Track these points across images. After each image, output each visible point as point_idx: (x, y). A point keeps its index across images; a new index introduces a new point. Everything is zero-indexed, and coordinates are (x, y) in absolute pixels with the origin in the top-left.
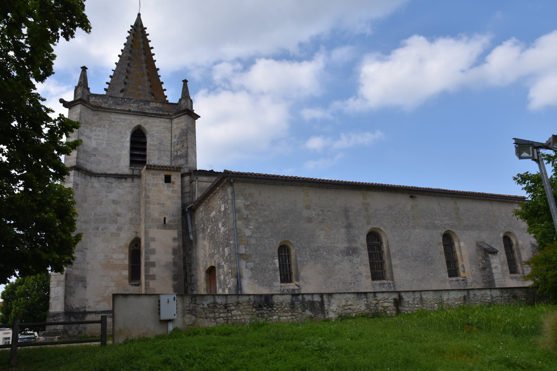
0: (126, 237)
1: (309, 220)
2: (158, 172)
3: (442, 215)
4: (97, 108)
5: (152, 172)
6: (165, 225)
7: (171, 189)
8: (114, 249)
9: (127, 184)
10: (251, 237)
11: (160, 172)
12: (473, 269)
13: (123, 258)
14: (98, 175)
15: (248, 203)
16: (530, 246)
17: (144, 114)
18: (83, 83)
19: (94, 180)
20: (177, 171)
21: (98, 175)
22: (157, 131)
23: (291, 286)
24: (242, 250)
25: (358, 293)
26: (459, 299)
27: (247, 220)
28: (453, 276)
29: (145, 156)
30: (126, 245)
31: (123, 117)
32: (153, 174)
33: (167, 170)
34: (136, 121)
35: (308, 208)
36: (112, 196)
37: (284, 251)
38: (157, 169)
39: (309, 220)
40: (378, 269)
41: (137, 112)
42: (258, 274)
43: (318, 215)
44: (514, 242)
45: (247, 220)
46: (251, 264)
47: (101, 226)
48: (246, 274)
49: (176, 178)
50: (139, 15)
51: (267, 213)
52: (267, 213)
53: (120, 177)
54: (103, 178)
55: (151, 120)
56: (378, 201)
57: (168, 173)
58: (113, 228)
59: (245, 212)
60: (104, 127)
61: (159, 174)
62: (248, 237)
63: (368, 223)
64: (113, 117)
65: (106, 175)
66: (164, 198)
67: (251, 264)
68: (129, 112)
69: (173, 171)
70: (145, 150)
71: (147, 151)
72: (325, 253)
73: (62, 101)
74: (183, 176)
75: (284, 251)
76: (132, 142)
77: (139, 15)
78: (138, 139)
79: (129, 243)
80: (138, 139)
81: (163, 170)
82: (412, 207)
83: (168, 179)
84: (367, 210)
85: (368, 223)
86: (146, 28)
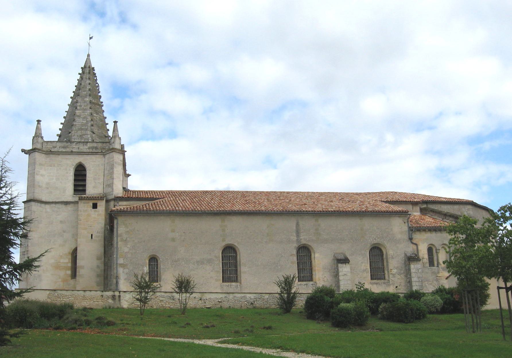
0: (68, 249)
2: (87, 201)
4: (49, 153)
5: (83, 201)
6: (28, 257)
7: (97, 213)
8: (61, 256)
9: (70, 208)
10: (128, 252)
11: (89, 201)
12: (325, 275)
13: (67, 261)
15: (128, 230)
16: (403, 255)
18: (38, 135)
19: (47, 206)
20: (101, 200)
22: (94, 166)
26: (404, 303)
28: (226, 282)
30: (69, 253)
32: (84, 203)
33: (94, 199)
35: (173, 231)
38: (86, 199)
39: (173, 240)
41: (78, 152)
44: (384, 253)
49: (102, 205)
53: (66, 203)
54: (54, 205)
55: (89, 157)
57: (95, 202)
60: (54, 166)
61: (89, 203)
62: (126, 252)
63: (224, 240)
64: (60, 158)
66: (96, 219)
67: (126, 271)
68: (72, 153)
69: (99, 199)
71: (87, 181)
72: (183, 263)
73: (23, 151)
74: (108, 201)
76: (75, 175)
78: (80, 174)
79: (71, 251)
80: (80, 174)
81: (91, 199)
83: (95, 206)
84: (224, 230)
86: (71, 98)
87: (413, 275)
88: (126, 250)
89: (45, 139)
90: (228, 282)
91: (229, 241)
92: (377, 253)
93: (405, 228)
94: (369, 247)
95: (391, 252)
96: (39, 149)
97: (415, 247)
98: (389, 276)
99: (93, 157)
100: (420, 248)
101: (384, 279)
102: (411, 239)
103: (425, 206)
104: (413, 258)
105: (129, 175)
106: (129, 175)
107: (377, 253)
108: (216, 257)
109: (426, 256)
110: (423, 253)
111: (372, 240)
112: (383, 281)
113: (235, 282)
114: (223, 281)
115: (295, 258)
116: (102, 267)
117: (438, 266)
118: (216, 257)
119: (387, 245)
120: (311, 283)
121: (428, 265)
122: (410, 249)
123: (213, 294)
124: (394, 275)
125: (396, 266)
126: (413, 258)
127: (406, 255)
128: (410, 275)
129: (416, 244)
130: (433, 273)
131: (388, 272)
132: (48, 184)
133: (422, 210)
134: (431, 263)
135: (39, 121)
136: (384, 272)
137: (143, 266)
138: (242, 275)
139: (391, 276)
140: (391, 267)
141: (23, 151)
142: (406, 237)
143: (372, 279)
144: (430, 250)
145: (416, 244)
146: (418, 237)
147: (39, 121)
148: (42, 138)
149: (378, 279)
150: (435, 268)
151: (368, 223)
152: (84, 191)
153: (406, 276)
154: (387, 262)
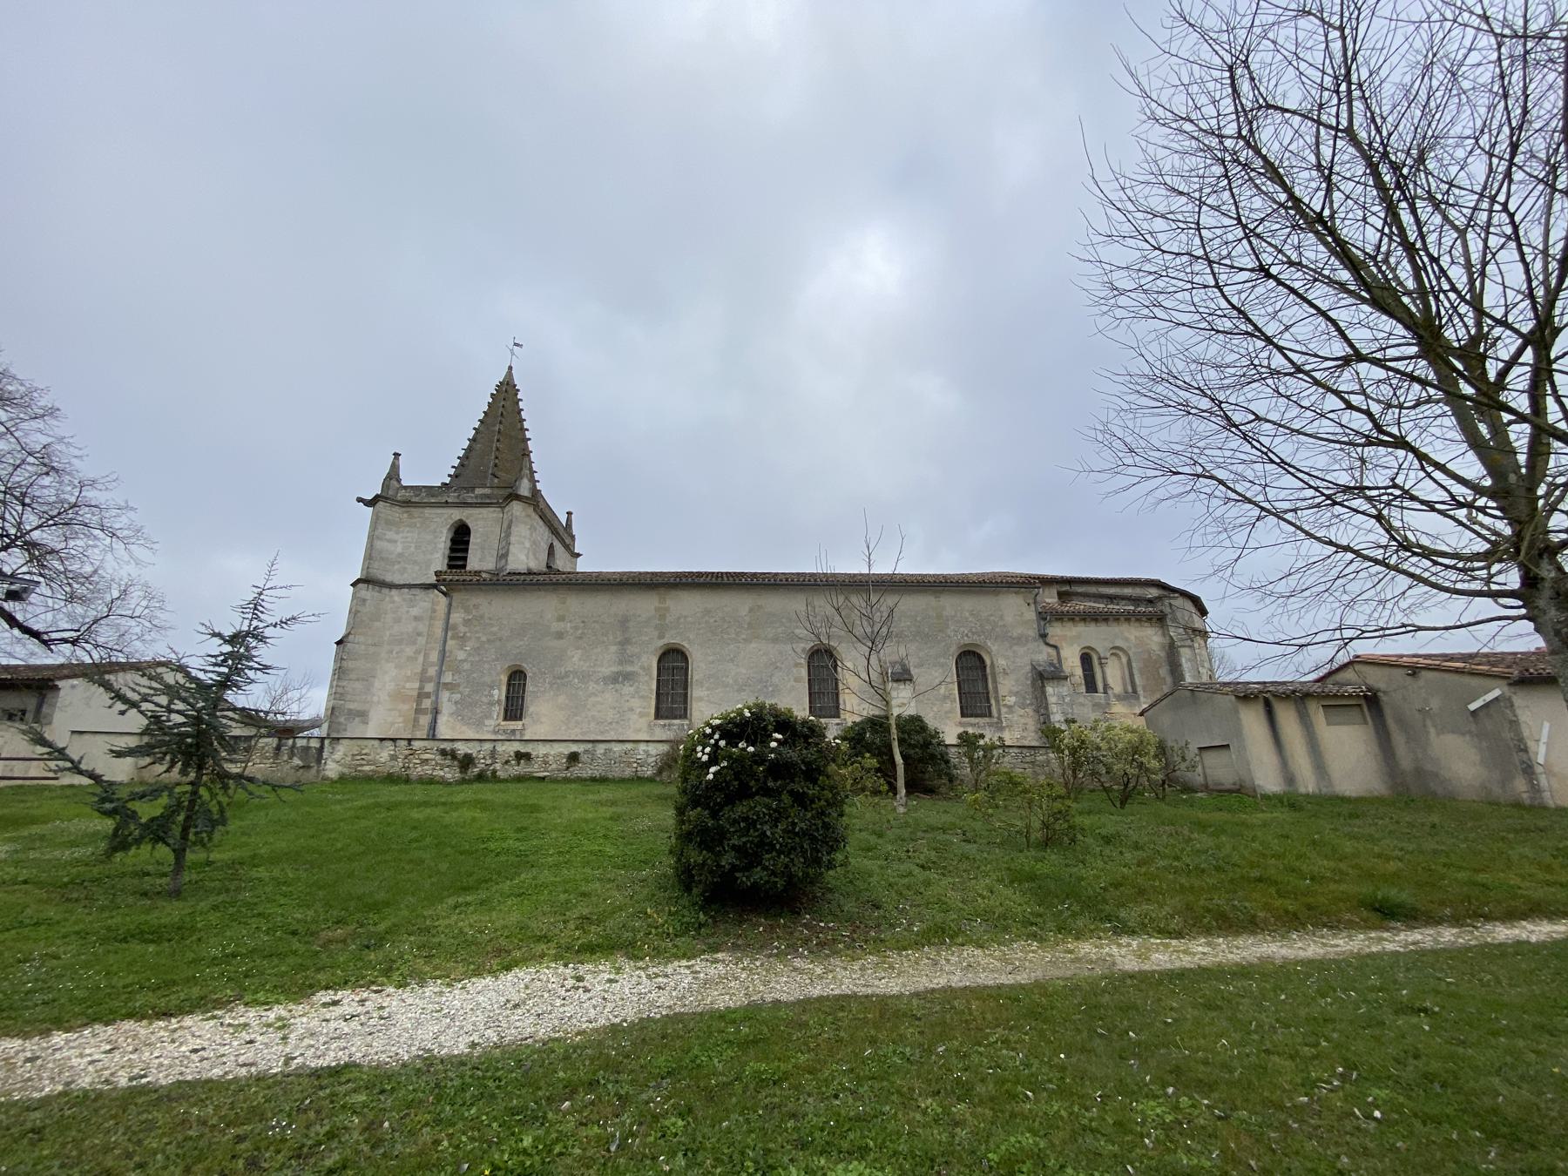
1: (560, 635)
3: (963, 614)
14: (391, 586)
16: (1029, 668)
17: (465, 505)
19: (394, 592)
21: (391, 586)
23: (516, 725)
24: (448, 678)
25: (382, 740)
27: (463, 639)
29: (465, 559)
31: (439, 511)
34: (457, 514)
35: (561, 619)
36: (415, 611)
37: (517, 678)
39: (560, 635)
40: (514, 710)
42: (464, 710)
43: (576, 628)
44: (988, 662)
45: (463, 639)
46: (457, 696)
47: (397, 649)
48: (446, 708)
50: (510, 368)
51: (495, 629)
52: (495, 629)
56: (687, 604)
58: (409, 651)
59: (462, 629)
63: (661, 637)
64: (427, 511)
65: (410, 586)
67: (457, 696)
70: (466, 550)
73: (360, 500)
75: (517, 678)
77: (510, 368)
78: (461, 537)
80: (461, 537)
82: (751, 610)
84: (663, 617)
85: (661, 637)
87: (1054, 708)
88: (461, 655)
89: (404, 483)
90: (667, 718)
91: (672, 639)
92: (972, 664)
93: (1031, 615)
94: (954, 651)
95: (1001, 662)
96: (393, 497)
97: (1052, 651)
98: (999, 711)
99: (484, 511)
100: (1064, 653)
101: (990, 715)
102: (1043, 636)
103: (1066, 588)
104: (1045, 676)
105: (578, 555)
106: (578, 555)
107: (972, 664)
108: (643, 668)
109: (1079, 672)
110: (1071, 662)
111: (958, 637)
112: (987, 720)
113: (680, 717)
114: (658, 716)
115: (804, 672)
116: (1228, 786)
117: (1105, 692)
118: (643, 668)
119: (994, 647)
120: (837, 721)
121: (1083, 689)
122: (1043, 655)
123: (556, 745)
124: (1010, 707)
125: (1015, 689)
126: (1045, 676)
127: (1034, 667)
128: (1047, 708)
129: (1055, 647)
130: (1096, 705)
131: (997, 701)
132: (400, 555)
133: (1061, 595)
134: (1091, 686)
135: (397, 455)
136: (988, 700)
137: (492, 688)
138: (695, 705)
139: (1004, 710)
140: (1002, 691)
141: (360, 500)
142: (1032, 632)
143: (963, 715)
144: (1086, 660)
145: (1055, 647)
146: (1056, 631)
147: (397, 455)
148: (399, 481)
149: (977, 716)
150: (1100, 695)
151: (950, 604)
152: (464, 566)
153: (1037, 711)
154: (995, 681)
